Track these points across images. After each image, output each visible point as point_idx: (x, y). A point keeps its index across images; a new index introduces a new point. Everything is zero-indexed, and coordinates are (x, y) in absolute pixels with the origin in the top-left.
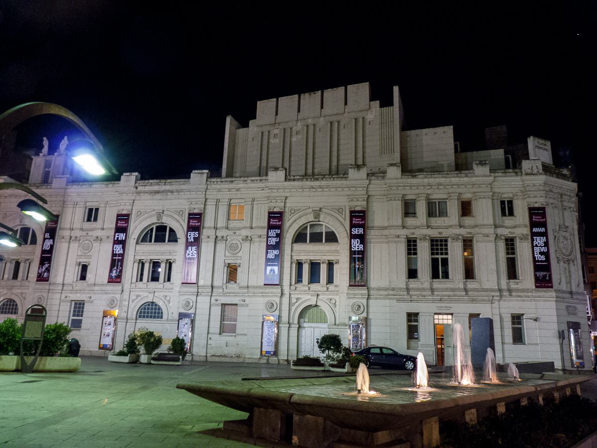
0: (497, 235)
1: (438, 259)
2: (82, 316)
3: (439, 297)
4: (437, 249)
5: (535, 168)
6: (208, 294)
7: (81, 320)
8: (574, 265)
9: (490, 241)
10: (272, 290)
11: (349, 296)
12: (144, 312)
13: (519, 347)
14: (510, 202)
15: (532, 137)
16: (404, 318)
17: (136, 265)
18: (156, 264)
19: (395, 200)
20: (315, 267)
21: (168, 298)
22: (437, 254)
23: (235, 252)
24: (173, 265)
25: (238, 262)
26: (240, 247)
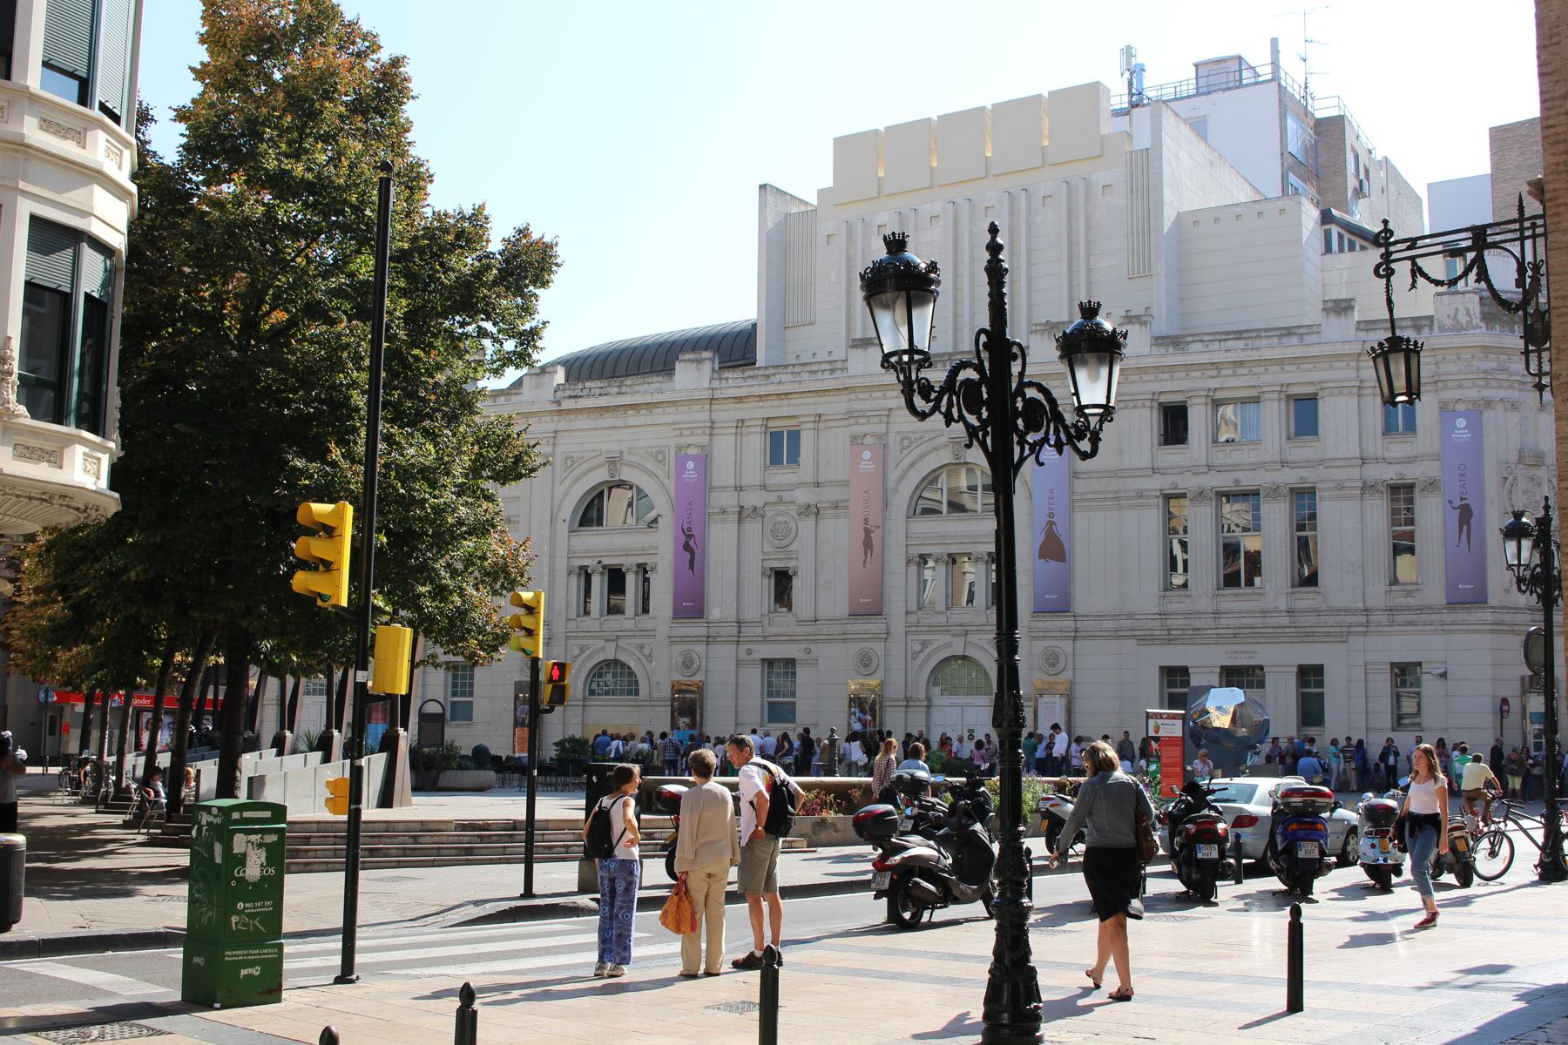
0: (1364, 483)
3: (1231, 631)
5: (1462, 311)
6: (989, 628)
7: (471, 703)
9: (1349, 497)
10: (866, 627)
11: (1034, 634)
14: (795, 436)
17: (574, 579)
18: (616, 579)
19: (1135, 407)
21: (647, 651)
23: (786, 542)
25: (791, 564)
26: (794, 530)
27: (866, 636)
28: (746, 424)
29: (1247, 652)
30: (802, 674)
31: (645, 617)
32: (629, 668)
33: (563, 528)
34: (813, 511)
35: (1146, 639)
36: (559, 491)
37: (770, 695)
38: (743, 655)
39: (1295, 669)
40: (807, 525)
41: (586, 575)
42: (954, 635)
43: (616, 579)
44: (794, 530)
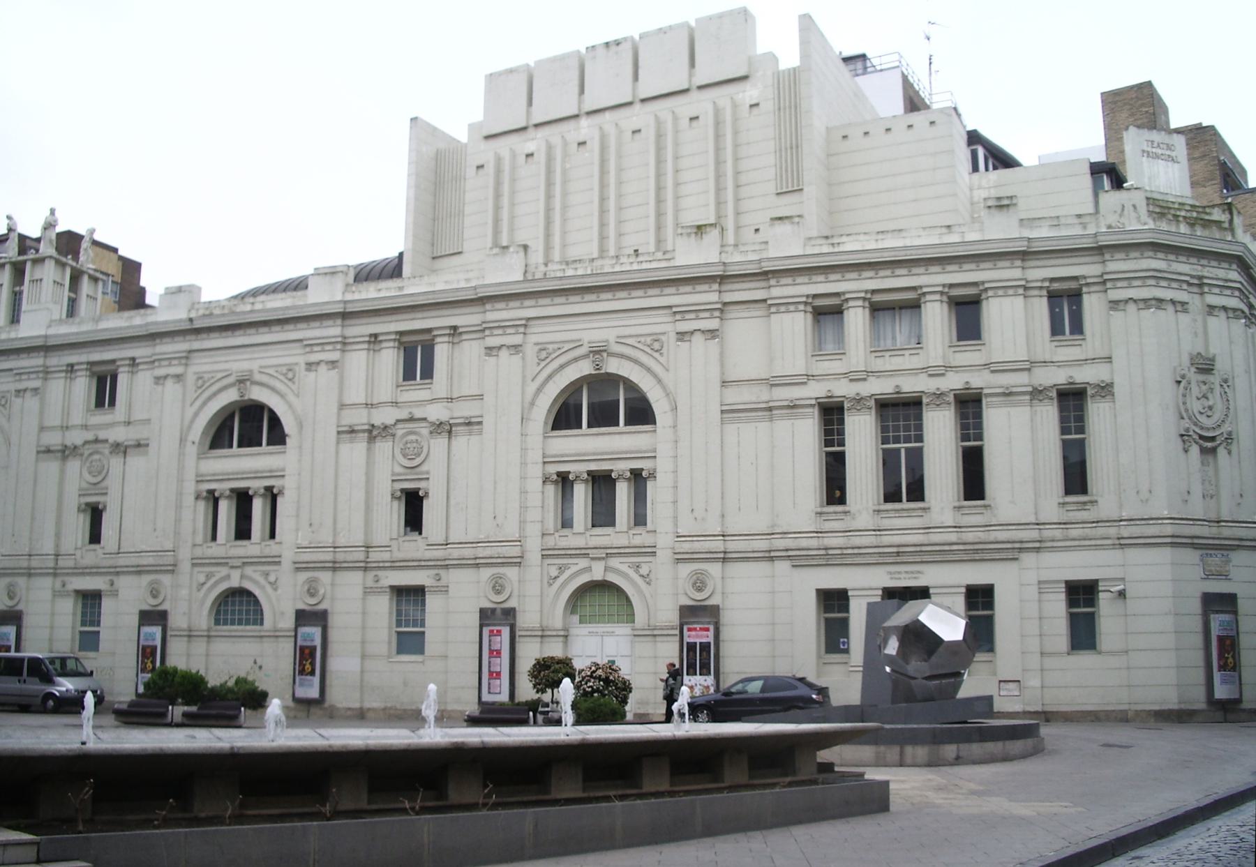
1: (898, 450)
2: (99, 625)
4: (896, 429)
8: (1230, 453)
12: (226, 612)
13: (1085, 659)
15: (1132, 129)
16: (475, 620)
17: (202, 505)
18: (243, 500)
20: (602, 483)
21: (272, 578)
22: (897, 440)
24: (280, 500)
27: (499, 561)
28: (76, 368)
29: (912, 572)
30: (432, 602)
31: (271, 542)
32: (255, 596)
33: (192, 451)
34: (445, 429)
35: (800, 560)
36: (190, 412)
37: (399, 624)
38: (370, 583)
39: (963, 590)
40: (438, 445)
41: (213, 499)
42: (593, 559)
43: (243, 500)
44: (425, 450)
